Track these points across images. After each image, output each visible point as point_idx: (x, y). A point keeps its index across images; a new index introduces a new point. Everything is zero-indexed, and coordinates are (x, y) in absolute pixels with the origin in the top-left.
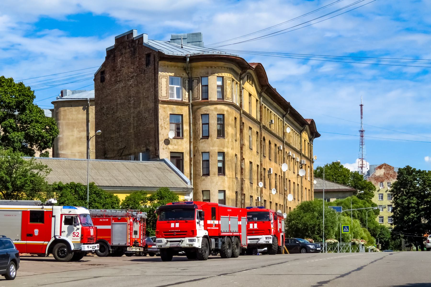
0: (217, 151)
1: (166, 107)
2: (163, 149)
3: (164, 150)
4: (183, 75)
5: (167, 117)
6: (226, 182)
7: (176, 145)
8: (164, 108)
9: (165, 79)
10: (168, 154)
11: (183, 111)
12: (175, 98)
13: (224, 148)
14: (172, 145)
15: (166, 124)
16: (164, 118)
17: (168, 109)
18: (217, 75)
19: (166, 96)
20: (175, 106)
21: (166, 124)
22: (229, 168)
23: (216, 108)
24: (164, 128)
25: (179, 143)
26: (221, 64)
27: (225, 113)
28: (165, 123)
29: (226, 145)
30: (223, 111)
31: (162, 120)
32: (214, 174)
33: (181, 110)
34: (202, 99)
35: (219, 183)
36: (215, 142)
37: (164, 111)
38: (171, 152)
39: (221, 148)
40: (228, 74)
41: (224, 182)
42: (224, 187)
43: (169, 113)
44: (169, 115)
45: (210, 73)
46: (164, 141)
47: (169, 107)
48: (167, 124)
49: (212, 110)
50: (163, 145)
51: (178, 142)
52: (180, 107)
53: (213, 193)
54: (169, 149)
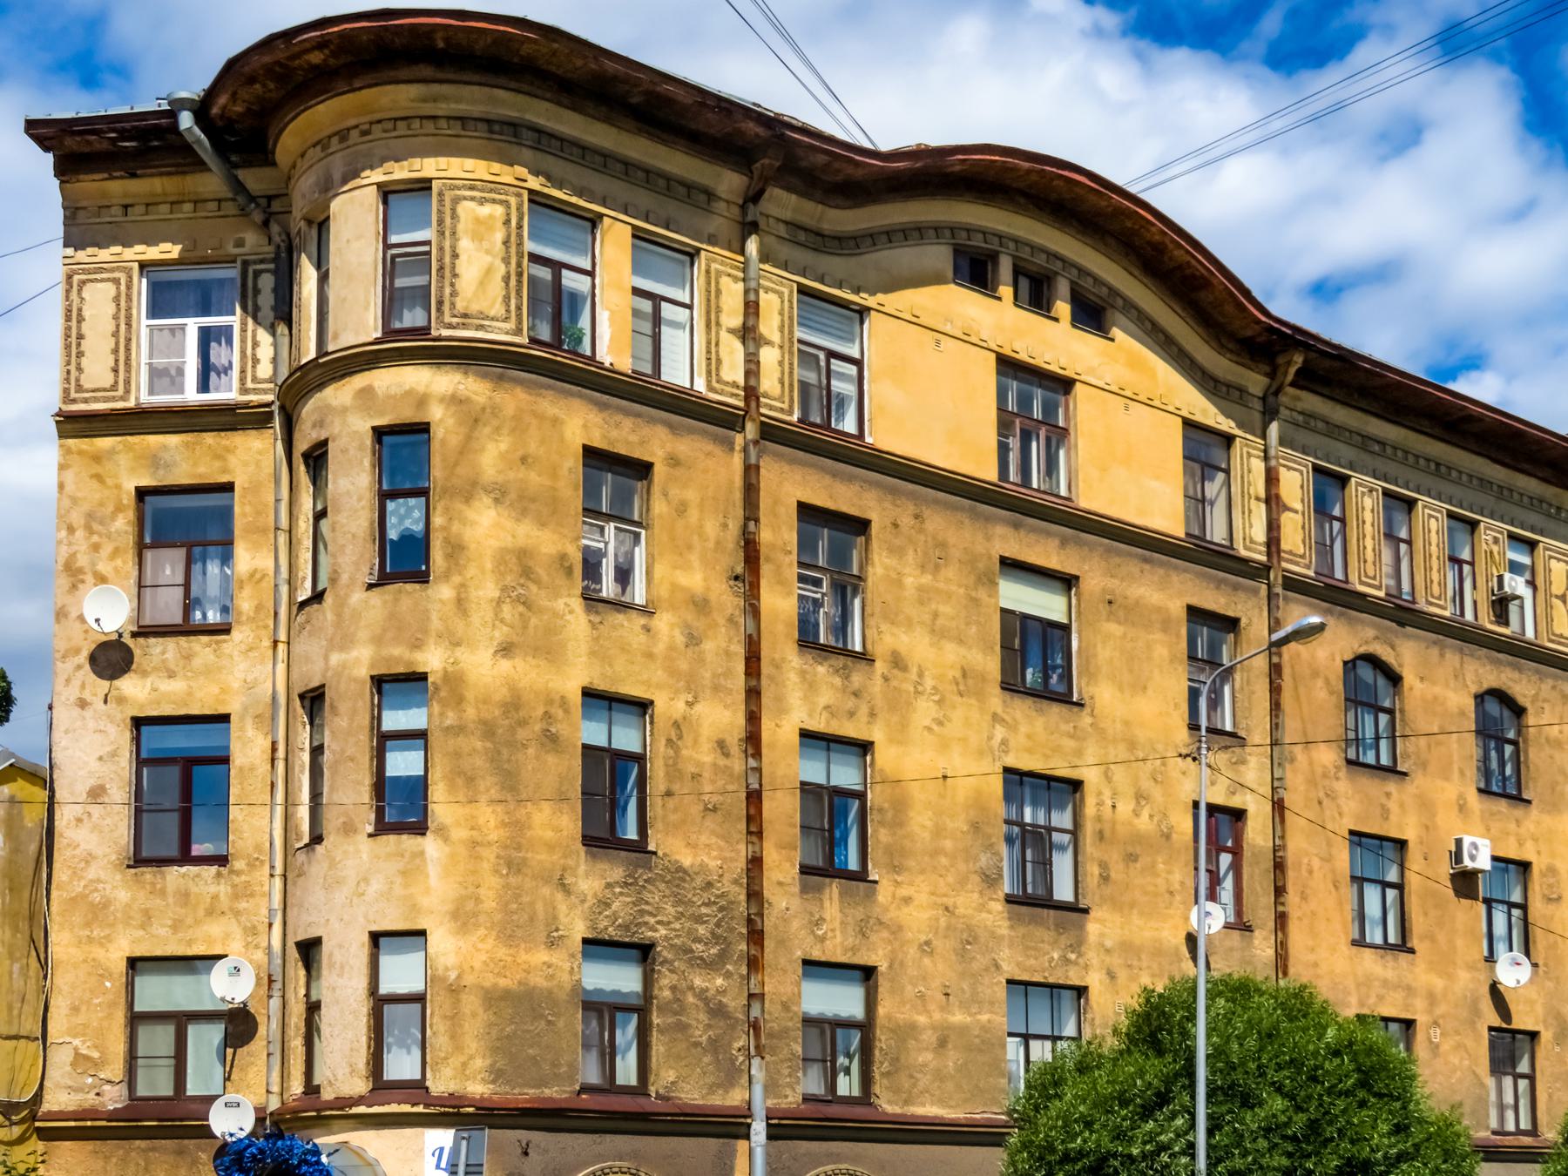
0: (364, 672)
1: (112, 452)
2: (83, 704)
3: (88, 713)
4: (240, 243)
5: (119, 509)
6: (433, 871)
7: (171, 675)
8: (97, 458)
9: (110, 289)
10: (112, 730)
11: (233, 461)
12: (191, 395)
13: (417, 645)
14: (144, 674)
15: (107, 549)
16: (90, 516)
17: (124, 460)
18: (377, 176)
19: (114, 387)
20: (173, 440)
21: (107, 549)
22: (470, 780)
23: (367, 392)
24: (89, 578)
25: (197, 662)
26: (398, 96)
27: (436, 414)
28: (96, 548)
29: (436, 624)
30: (422, 401)
31: (80, 534)
32: (349, 829)
33: (218, 457)
34: (183, 328)
35: (375, 886)
36: (356, 616)
37: (98, 478)
38: (138, 723)
39: (397, 651)
40: (469, 163)
41: (413, 870)
42: (415, 908)
43: (130, 485)
44: (129, 498)
45: (337, 176)
46: (93, 659)
47: (130, 448)
48: (116, 552)
49: (344, 410)
50: (76, 683)
51: (188, 657)
52: (209, 438)
53: (338, 957)
54: (121, 700)
